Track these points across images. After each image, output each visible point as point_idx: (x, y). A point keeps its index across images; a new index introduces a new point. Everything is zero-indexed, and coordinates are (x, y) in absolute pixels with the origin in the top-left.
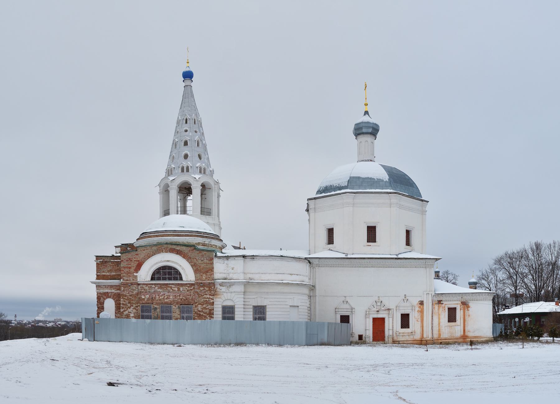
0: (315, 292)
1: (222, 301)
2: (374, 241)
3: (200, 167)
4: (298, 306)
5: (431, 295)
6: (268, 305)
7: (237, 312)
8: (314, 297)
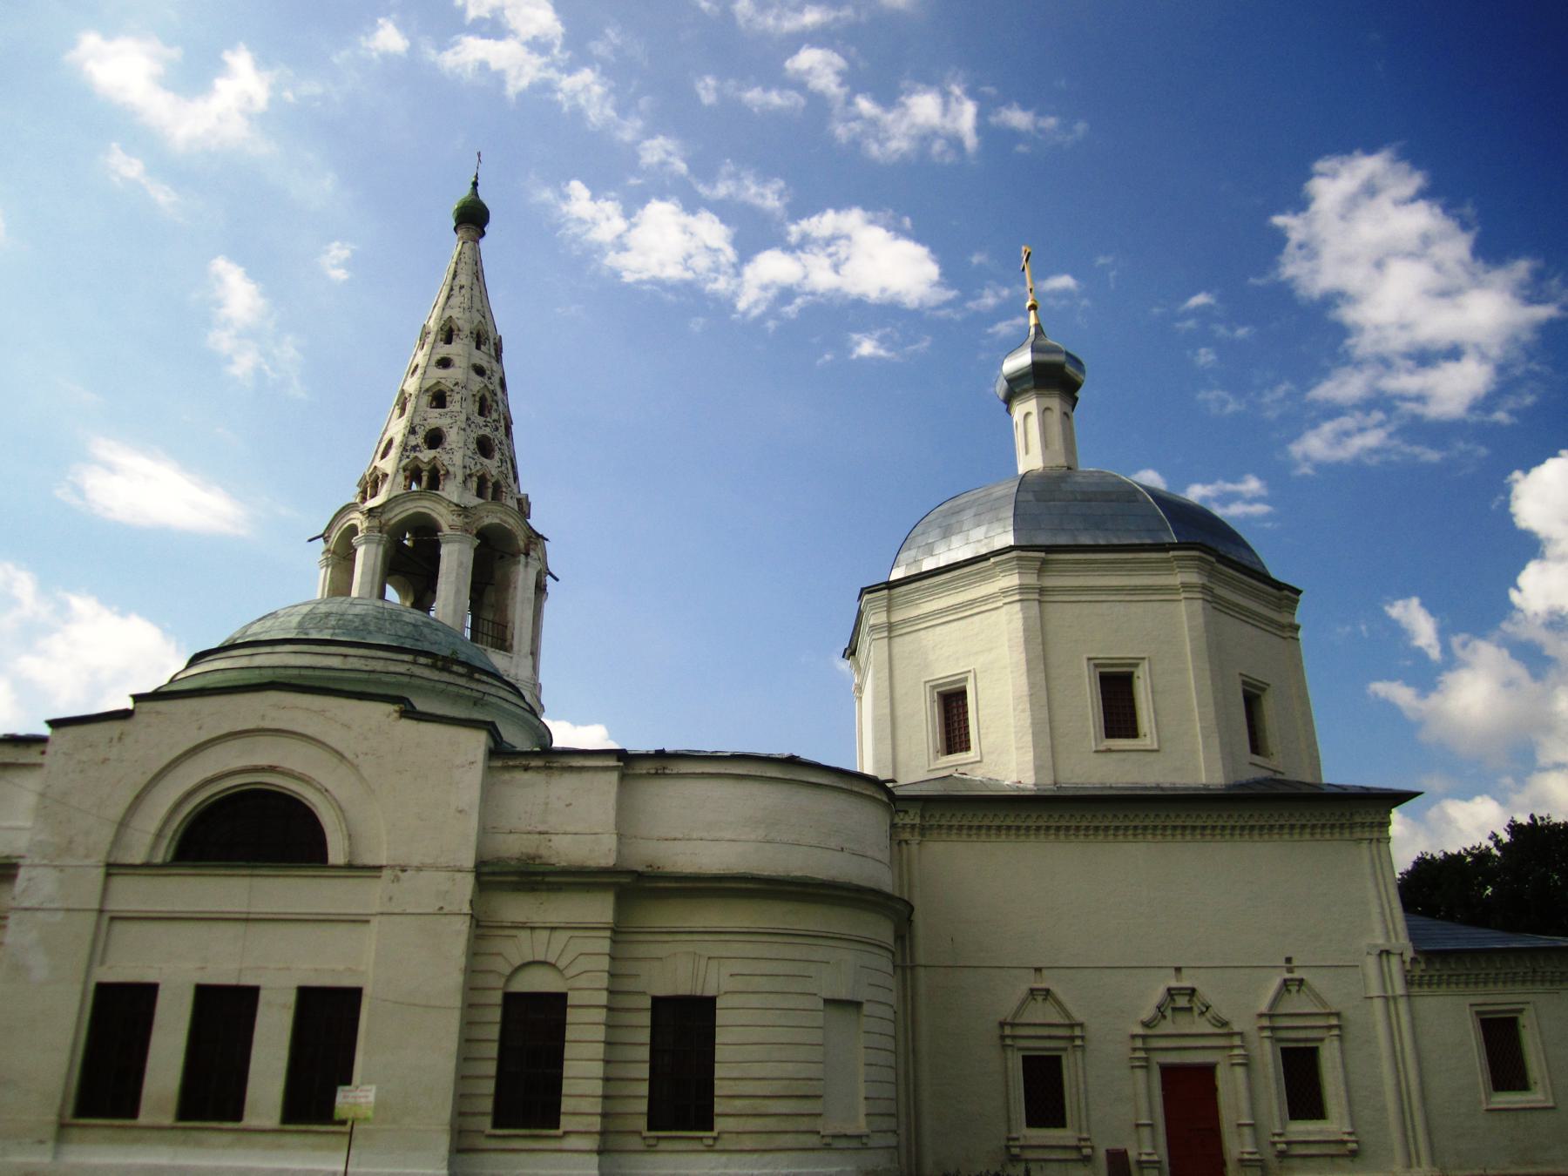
0: (911, 947)
1: (508, 970)
3: (479, 478)
4: (857, 1005)
5: (1395, 961)
6: (726, 993)
7: (574, 1010)
8: (908, 972)
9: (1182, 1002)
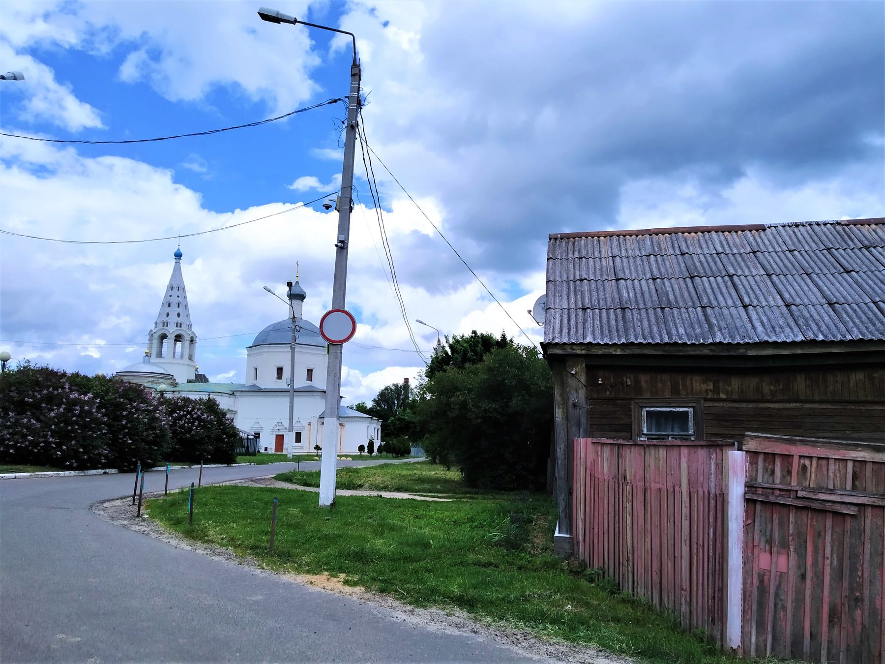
2: (405, 379)
9: (280, 424)
